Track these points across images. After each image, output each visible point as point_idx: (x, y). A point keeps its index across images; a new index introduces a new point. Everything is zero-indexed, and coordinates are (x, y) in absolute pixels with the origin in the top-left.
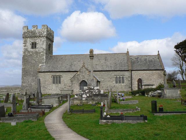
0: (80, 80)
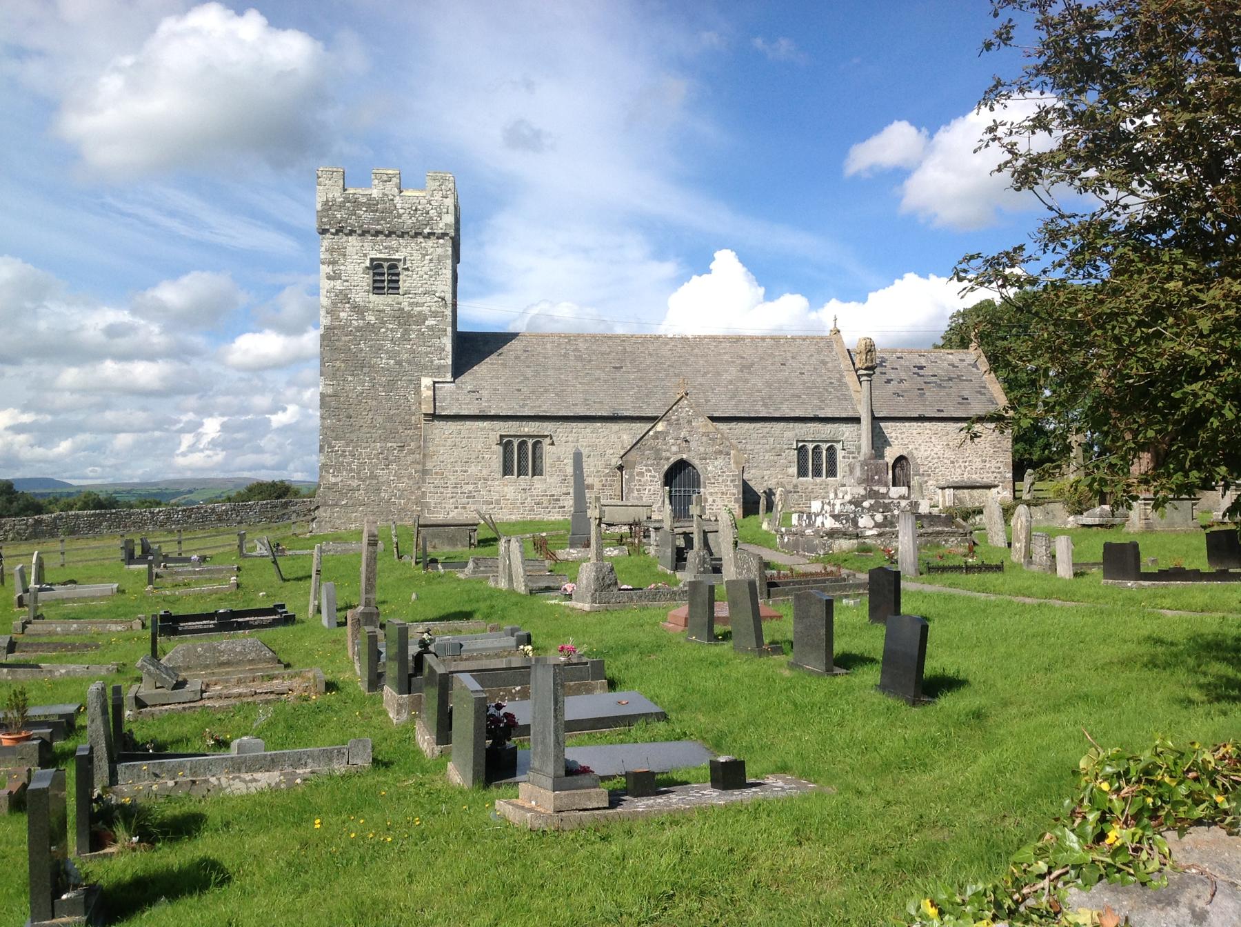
0: (668, 459)
